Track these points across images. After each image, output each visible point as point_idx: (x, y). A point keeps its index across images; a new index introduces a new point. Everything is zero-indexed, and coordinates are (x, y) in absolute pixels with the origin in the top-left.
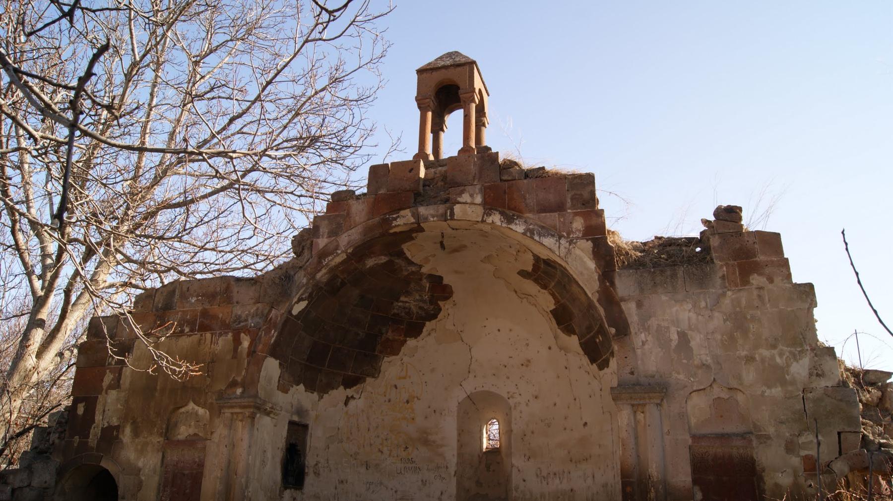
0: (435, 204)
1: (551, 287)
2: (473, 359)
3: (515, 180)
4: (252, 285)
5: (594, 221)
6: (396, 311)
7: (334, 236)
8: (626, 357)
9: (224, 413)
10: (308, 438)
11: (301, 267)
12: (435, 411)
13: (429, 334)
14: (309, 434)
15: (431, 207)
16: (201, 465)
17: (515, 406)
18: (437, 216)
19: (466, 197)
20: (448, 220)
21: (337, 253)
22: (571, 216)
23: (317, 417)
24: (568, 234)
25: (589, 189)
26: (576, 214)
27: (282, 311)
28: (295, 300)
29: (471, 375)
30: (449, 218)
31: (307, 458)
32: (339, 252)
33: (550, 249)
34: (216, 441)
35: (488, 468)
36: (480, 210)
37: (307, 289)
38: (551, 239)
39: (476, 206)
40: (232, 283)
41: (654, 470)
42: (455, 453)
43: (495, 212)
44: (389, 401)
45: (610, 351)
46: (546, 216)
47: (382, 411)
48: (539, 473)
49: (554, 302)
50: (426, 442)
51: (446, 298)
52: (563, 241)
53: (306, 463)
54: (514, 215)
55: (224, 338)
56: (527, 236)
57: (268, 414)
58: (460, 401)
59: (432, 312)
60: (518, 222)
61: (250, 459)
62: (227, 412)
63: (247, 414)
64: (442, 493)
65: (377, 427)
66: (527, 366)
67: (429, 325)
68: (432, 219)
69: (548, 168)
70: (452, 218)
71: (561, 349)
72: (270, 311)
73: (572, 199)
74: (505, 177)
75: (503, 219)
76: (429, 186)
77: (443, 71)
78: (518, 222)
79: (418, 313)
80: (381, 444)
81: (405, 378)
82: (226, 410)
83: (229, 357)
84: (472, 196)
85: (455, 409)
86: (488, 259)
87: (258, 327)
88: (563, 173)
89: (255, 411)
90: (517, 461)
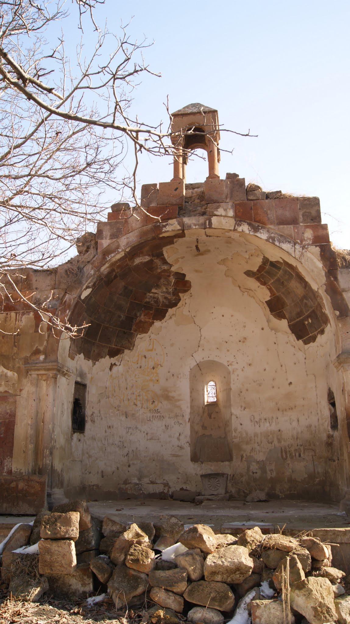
0: (195, 216)
1: (269, 283)
2: (202, 338)
3: (258, 200)
4: (48, 275)
5: (321, 232)
6: (147, 300)
7: (115, 238)
8: (348, 333)
9: (31, 375)
10: (87, 394)
11: (89, 262)
12: (173, 375)
13: (171, 318)
14: (87, 392)
15: (193, 217)
16: (13, 416)
17: (233, 371)
18: (198, 225)
19: (220, 211)
20: (207, 228)
21: (118, 251)
22: (303, 228)
23: (92, 378)
24: (302, 241)
25: (316, 208)
26: (307, 227)
27: (74, 296)
28: (84, 287)
29: (200, 349)
30: (208, 226)
31: (86, 410)
32: (120, 250)
33: (288, 252)
34: (25, 396)
35: (210, 416)
36: (233, 221)
37: (93, 279)
38: (289, 245)
39: (229, 218)
40: (31, 273)
42: (189, 405)
43: (244, 223)
44: (141, 367)
45: (321, 328)
46: (284, 227)
47: (136, 375)
48: (252, 419)
49: (270, 295)
50: (167, 398)
51: (185, 291)
52: (297, 246)
53: (86, 413)
54: (258, 226)
55: (27, 316)
56: (270, 242)
57: (64, 375)
58: (191, 367)
59: (174, 301)
60: (262, 231)
61: (55, 410)
62: (34, 374)
63: (51, 375)
64: (180, 435)
65: (132, 387)
66: (244, 342)
67: (170, 311)
68: (194, 227)
69: (283, 192)
70: (210, 227)
71: (272, 329)
72: (65, 295)
73: (303, 215)
74: (251, 197)
75: (250, 229)
76: (188, 203)
77: (192, 116)
78: (262, 231)
79: (163, 302)
80: (136, 399)
81: (152, 350)
82: (33, 373)
83: (31, 331)
84: (225, 210)
85: (188, 373)
86: (223, 262)
87: (55, 308)
88: (295, 196)
89: (57, 373)
90: (236, 411)
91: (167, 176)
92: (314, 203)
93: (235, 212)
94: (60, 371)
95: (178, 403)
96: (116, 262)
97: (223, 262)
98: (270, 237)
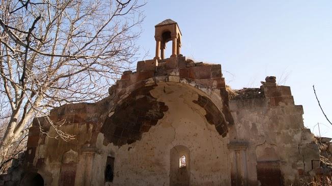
5: (221, 82)
16: (74, 173)
19: (173, 73)
26: (214, 80)
36: (179, 78)
41: (243, 175)
42: (169, 168)
50: (158, 164)
52: (209, 90)
62: (84, 153)
70: (168, 81)
73: (213, 74)
74: (188, 66)
81: (150, 140)
83: (85, 133)
84: (175, 73)
86: (181, 96)
90: (192, 171)
91: (151, 57)
92: (219, 67)
93: (180, 74)
94: (97, 151)
95: (164, 167)
96: (125, 99)
97: (181, 96)
98: (196, 85)
